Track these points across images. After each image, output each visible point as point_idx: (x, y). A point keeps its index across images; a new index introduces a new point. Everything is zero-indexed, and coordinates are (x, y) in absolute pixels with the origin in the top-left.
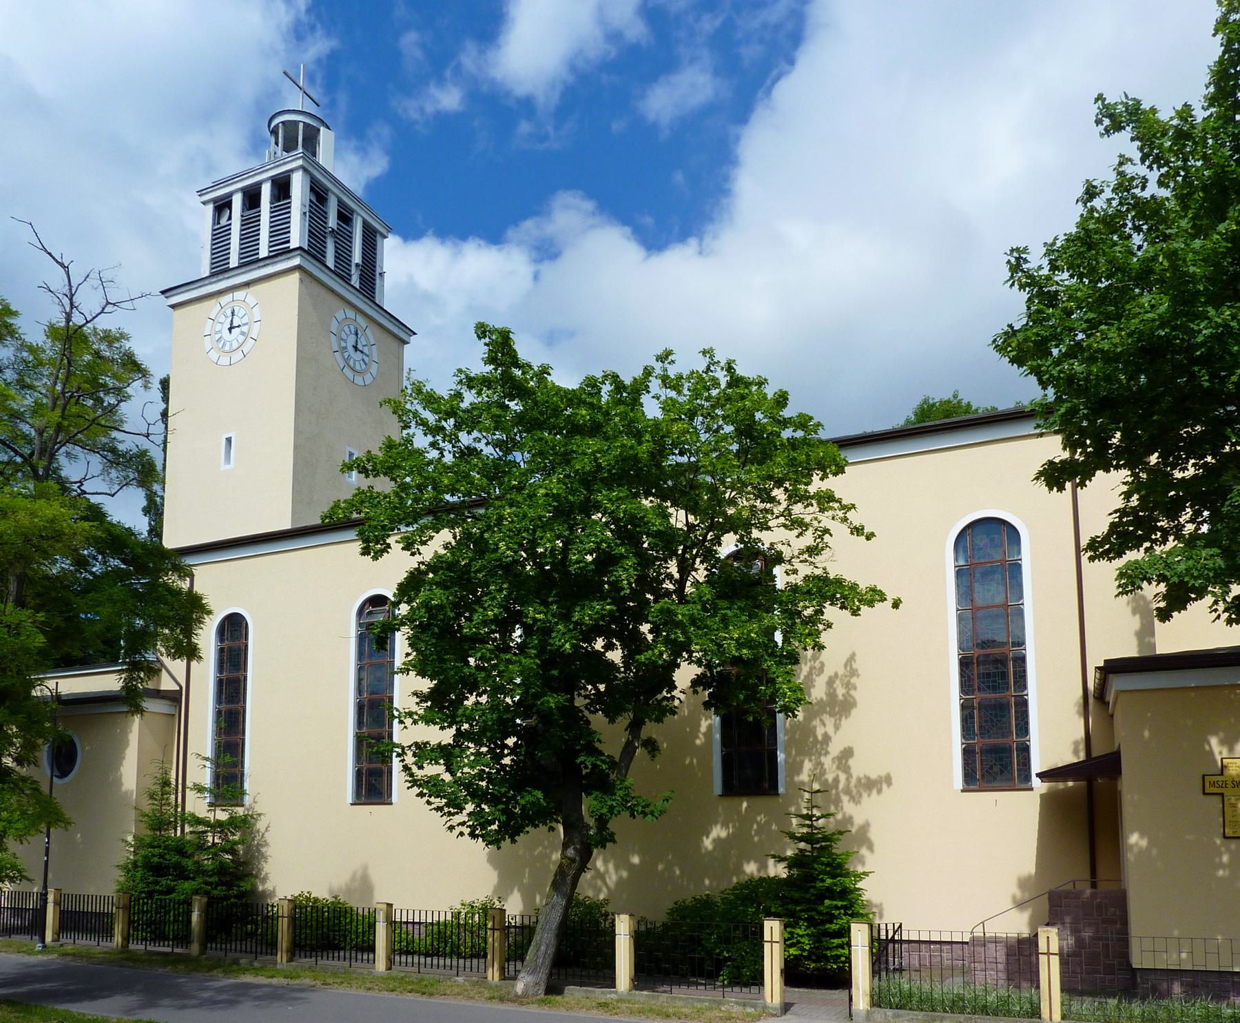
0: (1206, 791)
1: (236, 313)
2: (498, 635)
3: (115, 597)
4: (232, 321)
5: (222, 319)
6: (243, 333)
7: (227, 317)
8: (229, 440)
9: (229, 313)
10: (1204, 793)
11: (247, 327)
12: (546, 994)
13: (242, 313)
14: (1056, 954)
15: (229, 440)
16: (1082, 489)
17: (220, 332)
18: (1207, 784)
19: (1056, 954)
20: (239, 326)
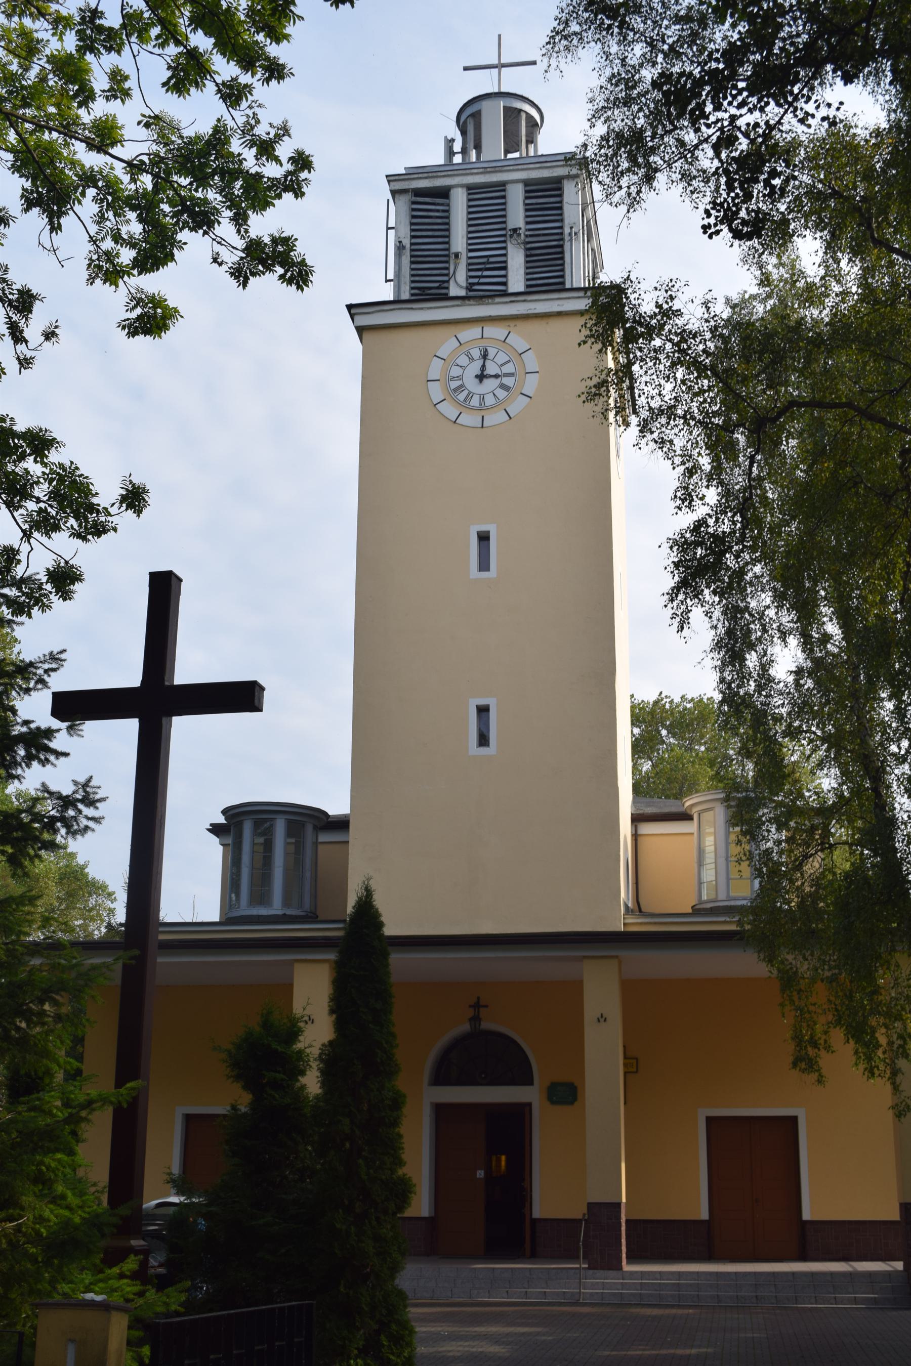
0: (635, 1070)
1: (491, 356)
2: (834, 543)
3: (759, 574)
4: (484, 366)
5: (463, 360)
6: (503, 387)
7: (472, 359)
8: (484, 538)
9: (476, 353)
10: (637, 1059)
11: (459, 362)
12: (530, 1083)
13: (502, 358)
14: (717, 894)
15: (484, 538)
16: (57, 233)
17: (460, 378)
18: (635, 1064)
19: (717, 894)
20: (496, 376)
